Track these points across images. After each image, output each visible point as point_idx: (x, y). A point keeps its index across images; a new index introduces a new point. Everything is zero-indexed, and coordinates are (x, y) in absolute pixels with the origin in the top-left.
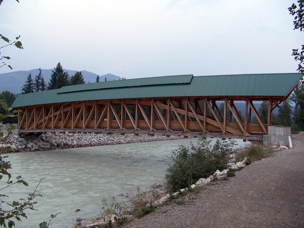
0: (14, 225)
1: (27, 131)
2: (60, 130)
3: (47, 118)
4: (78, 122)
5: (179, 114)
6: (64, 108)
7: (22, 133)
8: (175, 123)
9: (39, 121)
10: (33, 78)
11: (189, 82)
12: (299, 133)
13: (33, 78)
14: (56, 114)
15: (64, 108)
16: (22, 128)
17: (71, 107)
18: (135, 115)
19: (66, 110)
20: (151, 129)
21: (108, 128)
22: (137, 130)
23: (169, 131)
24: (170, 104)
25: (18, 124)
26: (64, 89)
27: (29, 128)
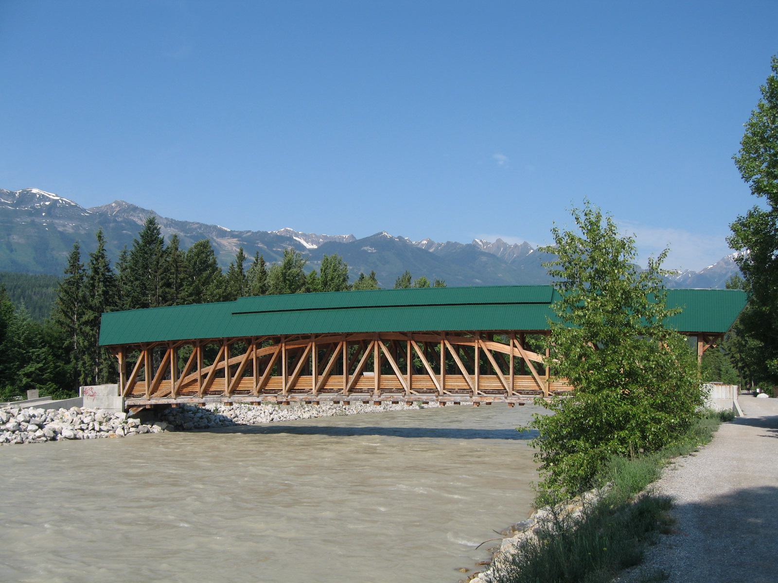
0: (687, 270)
1: (146, 401)
2: (251, 398)
3: (210, 369)
4: (133, 384)
5: (490, 351)
6: (257, 349)
7: (130, 406)
8: (523, 381)
9: (185, 376)
10: (85, 261)
11: (550, 301)
12: (755, 394)
13: (85, 261)
14: (234, 360)
15: (257, 349)
16: (129, 394)
17: (280, 345)
18: (170, 370)
19: (263, 351)
20: (477, 391)
21: (376, 391)
22: (444, 393)
23: (513, 394)
24: (514, 343)
25: (119, 386)
26: (242, 304)
27: (155, 394)
